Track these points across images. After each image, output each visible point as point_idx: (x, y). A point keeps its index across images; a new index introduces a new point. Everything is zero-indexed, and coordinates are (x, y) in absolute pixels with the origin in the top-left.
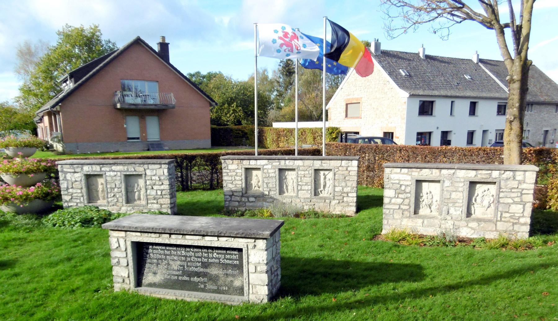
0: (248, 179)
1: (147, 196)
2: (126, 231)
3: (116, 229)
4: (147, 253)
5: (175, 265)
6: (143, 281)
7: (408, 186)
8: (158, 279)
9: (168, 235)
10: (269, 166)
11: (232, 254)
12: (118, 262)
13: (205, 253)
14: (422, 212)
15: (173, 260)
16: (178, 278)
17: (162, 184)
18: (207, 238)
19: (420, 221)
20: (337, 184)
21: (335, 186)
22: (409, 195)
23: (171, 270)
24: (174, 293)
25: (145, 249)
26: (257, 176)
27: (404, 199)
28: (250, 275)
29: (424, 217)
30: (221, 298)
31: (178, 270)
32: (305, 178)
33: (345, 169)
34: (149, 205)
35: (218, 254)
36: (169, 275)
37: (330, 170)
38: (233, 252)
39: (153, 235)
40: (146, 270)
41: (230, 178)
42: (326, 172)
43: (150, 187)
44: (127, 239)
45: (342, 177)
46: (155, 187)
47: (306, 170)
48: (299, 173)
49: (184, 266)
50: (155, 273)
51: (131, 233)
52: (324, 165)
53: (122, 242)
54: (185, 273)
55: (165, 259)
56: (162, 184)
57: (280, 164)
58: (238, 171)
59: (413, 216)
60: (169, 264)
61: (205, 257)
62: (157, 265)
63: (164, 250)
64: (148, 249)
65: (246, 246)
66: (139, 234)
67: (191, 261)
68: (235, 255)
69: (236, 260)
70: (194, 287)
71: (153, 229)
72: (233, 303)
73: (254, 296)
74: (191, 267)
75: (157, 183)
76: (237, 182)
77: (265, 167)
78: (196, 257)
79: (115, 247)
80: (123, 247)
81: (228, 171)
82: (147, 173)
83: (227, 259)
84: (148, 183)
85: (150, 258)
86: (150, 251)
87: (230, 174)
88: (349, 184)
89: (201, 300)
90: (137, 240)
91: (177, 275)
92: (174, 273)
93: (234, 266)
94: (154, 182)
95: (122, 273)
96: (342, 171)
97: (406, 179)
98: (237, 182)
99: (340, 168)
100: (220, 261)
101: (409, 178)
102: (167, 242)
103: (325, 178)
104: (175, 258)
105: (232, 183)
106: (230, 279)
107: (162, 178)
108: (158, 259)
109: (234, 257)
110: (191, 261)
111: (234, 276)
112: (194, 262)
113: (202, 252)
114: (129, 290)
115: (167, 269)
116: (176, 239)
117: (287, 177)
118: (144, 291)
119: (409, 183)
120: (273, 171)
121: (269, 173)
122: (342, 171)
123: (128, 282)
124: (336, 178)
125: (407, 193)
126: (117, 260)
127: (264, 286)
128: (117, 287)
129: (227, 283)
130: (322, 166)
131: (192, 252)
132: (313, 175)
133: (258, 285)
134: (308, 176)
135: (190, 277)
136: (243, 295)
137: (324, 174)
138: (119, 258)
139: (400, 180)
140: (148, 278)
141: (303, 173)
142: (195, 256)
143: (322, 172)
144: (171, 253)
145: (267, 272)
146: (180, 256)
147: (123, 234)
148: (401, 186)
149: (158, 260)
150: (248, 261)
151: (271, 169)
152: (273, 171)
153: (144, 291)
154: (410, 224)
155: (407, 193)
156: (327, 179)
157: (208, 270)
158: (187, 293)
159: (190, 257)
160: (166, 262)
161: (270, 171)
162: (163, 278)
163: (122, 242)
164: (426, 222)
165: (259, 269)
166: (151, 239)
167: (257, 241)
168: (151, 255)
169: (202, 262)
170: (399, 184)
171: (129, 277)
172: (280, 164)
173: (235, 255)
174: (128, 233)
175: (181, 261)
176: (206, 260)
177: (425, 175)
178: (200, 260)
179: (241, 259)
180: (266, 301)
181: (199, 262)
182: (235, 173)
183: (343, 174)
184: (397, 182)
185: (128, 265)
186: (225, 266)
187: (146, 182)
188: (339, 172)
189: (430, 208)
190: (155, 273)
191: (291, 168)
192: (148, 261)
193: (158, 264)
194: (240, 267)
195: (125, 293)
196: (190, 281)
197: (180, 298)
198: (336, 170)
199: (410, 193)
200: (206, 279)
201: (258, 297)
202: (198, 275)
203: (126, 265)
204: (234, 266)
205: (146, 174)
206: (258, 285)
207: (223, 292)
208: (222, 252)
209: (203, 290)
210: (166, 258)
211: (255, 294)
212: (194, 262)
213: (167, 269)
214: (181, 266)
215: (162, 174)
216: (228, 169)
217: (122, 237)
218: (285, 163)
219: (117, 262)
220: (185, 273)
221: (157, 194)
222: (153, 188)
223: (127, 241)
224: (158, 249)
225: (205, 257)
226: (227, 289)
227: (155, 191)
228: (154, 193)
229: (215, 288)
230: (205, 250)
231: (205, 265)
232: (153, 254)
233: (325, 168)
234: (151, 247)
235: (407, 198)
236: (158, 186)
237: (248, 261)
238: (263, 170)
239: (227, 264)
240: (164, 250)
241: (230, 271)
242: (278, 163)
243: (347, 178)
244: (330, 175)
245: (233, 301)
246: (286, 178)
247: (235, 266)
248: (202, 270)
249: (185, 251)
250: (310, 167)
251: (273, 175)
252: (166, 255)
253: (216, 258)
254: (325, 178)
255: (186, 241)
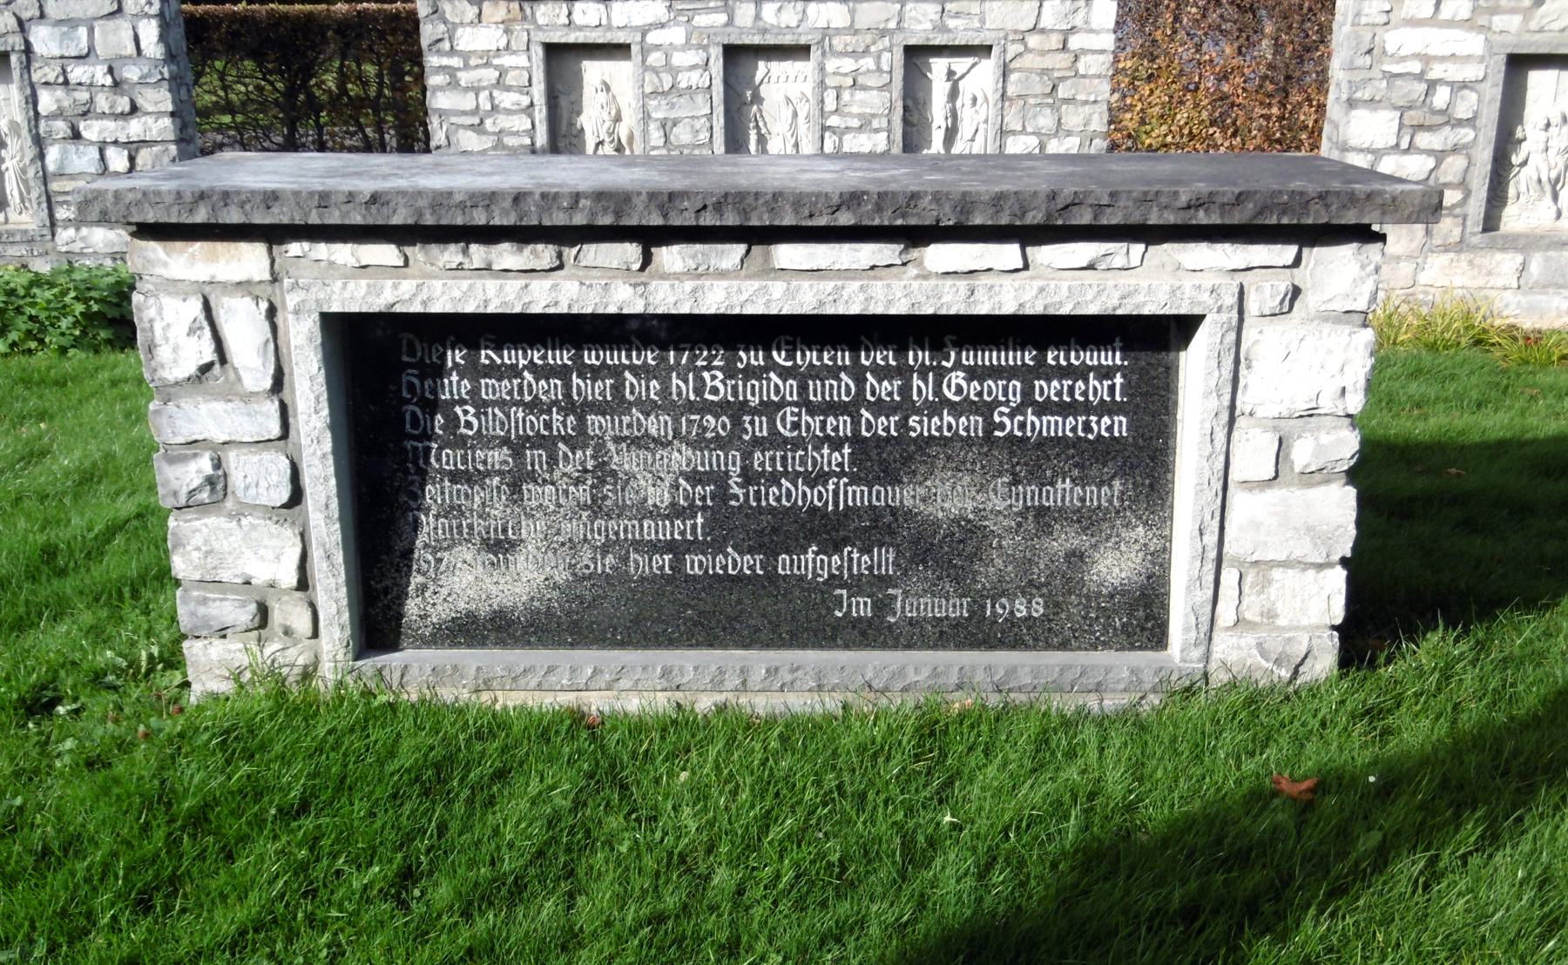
0: (563, 102)
1: (45, 181)
2: (273, 235)
3: (201, 216)
4: (432, 406)
5: (657, 476)
6: (412, 607)
7: (1464, 85)
8: (522, 581)
9: (630, 252)
10: (676, 35)
11: (1081, 373)
12: (217, 483)
13: (882, 373)
14: (1514, 218)
15: (640, 442)
16: (677, 565)
17: (134, 109)
18: (940, 256)
19: (1507, 263)
20: (1013, 123)
21: (1003, 133)
22: (1466, 134)
23: (621, 511)
24: (666, 673)
25: (410, 377)
26: (607, 87)
27: (1440, 156)
28: (1237, 498)
29: (1525, 244)
30: (1011, 671)
31: (676, 512)
32: (860, 95)
33: (1055, 41)
34: (65, 235)
35: (973, 374)
36: (605, 549)
37: (985, 50)
38: (1090, 358)
39: (506, 255)
40: (430, 527)
41: (468, 102)
42: (960, 64)
43: (61, 127)
44: (292, 300)
45: (1039, 86)
46: (92, 130)
47: (866, 52)
48: (831, 65)
49: (721, 479)
50: (500, 546)
51: (322, 250)
52: (951, 23)
53: (243, 327)
54: (727, 524)
55: (578, 440)
56: (134, 109)
57: (730, 22)
58: (507, 60)
59: (1477, 239)
60: (603, 473)
61: (879, 408)
62: (515, 487)
63: (563, 373)
64: (439, 371)
65: (1230, 299)
66: (384, 254)
67: (774, 441)
68: (1105, 373)
69: (1106, 409)
70: (806, 621)
71: (518, 198)
72: (1092, 702)
73: (1249, 640)
74: (774, 479)
75: (102, 103)
76: (504, 122)
77: (653, 38)
78: (812, 410)
79: (189, 368)
80: (252, 367)
81: (455, 62)
82: (39, 48)
83: (1043, 409)
84: (47, 101)
85: (461, 442)
86: (455, 385)
87: (464, 78)
88: (1073, 118)
89: (862, 703)
90: (376, 305)
91: (670, 546)
92: (650, 530)
93: (1090, 456)
94: (83, 96)
95: (249, 568)
96: (1043, 53)
97: (1461, 50)
98: (504, 122)
99: (1033, 41)
100: (990, 426)
101: (1474, 43)
102: (623, 299)
103: (954, 94)
104: (653, 426)
105: (479, 128)
106: (1064, 540)
107: (131, 73)
108: (518, 447)
109: (1098, 389)
110: (774, 441)
111: (1088, 519)
112: (798, 443)
113: (858, 374)
114: (307, 675)
115: (596, 508)
116: (694, 274)
117: (763, 91)
118: (413, 671)
119: (1472, 72)
120: (695, 57)
121: (674, 71)
122: (1043, 53)
123: (302, 624)
124: (1011, 90)
125: (1460, 123)
126: (204, 464)
127: (1320, 567)
128: (212, 667)
129: (1039, 573)
130: (943, 28)
131: (785, 374)
132: (899, 75)
133: (1285, 564)
134: (873, 81)
135: (772, 554)
136: (1156, 636)
137: (951, 73)
138: (218, 452)
139: (1427, 59)
140: (451, 580)
141: (848, 64)
142: (804, 403)
143: (939, 66)
144: (618, 389)
145: (1353, 476)
146: (690, 407)
147: (250, 259)
148: (1432, 85)
149: (517, 453)
150: (1232, 407)
151: (687, 45)
152: (695, 57)
153: (413, 671)
154: (1458, 282)
155: (1460, 123)
156: (964, 99)
157: (905, 496)
158: (759, 660)
159: (770, 409)
160: (576, 460)
161: (679, 59)
162: (562, 576)
163: (243, 327)
164: (1536, 265)
165: (1303, 454)
166: (491, 285)
167: (1317, 255)
168: (466, 413)
169: (856, 439)
170: (1420, 77)
171: (303, 584)
172: (730, 22)
173: (1105, 373)
174: (295, 248)
175: (699, 443)
176: (885, 425)
177: (1557, 26)
178: (844, 425)
179: (1153, 405)
180: (1324, 662)
181: (836, 444)
182: (490, 75)
183: (1044, 72)
184: (1415, 67)
185: (297, 497)
186: (1031, 459)
187: (33, 100)
188: (1029, 61)
189: (1555, 197)
190: (500, 546)
191: (787, 40)
192: (446, 458)
193: (516, 481)
194: (1143, 461)
195: (291, 702)
196: (772, 576)
197: (705, 703)
198: (1013, 49)
199: (1471, 122)
200: (884, 560)
201: (1275, 645)
202: (829, 529)
203: (284, 495)
204: (1090, 456)
205: (28, 50)
206: (1285, 564)
207: (1011, 636)
208: (1011, 358)
209: (870, 634)
210: (581, 426)
211: (1252, 626)
212: (798, 443)
213: (596, 508)
214: (695, 478)
215: (130, 49)
216: (453, 52)
217: (244, 287)
218: (758, 17)
219: (210, 481)
220: (727, 524)
221: (105, 171)
222: (76, 135)
223: (285, 318)
224: (514, 372)
225: (879, 408)
226: (1038, 610)
227: (94, 153)
228: (84, 160)
229: (955, 608)
230: (884, 357)
231: (881, 460)
232: (481, 406)
233: (960, 40)
234: (455, 356)
235: (1455, 150)
236: (110, 124)
237: (1232, 407)
238: (645, 52)
239: (1043, 443)
240: (563, 373)
241: (1064, 492)
242: (722, 18)
243: (1062, 92)
244: (981, 77)
245: (1098, 688)
246: (757, 99)
247: (1104, 449)
248: (856, 495)
249: (730, 372)
250: (883, 33)
251: (695, 78)
252: (579, 409)
253: (957, 409)
254: (954, 94)
255: (777, 288)
